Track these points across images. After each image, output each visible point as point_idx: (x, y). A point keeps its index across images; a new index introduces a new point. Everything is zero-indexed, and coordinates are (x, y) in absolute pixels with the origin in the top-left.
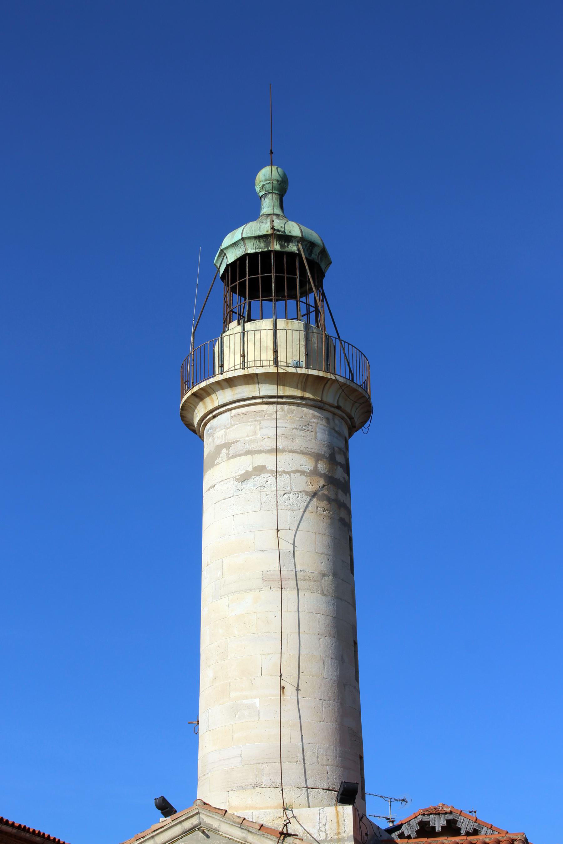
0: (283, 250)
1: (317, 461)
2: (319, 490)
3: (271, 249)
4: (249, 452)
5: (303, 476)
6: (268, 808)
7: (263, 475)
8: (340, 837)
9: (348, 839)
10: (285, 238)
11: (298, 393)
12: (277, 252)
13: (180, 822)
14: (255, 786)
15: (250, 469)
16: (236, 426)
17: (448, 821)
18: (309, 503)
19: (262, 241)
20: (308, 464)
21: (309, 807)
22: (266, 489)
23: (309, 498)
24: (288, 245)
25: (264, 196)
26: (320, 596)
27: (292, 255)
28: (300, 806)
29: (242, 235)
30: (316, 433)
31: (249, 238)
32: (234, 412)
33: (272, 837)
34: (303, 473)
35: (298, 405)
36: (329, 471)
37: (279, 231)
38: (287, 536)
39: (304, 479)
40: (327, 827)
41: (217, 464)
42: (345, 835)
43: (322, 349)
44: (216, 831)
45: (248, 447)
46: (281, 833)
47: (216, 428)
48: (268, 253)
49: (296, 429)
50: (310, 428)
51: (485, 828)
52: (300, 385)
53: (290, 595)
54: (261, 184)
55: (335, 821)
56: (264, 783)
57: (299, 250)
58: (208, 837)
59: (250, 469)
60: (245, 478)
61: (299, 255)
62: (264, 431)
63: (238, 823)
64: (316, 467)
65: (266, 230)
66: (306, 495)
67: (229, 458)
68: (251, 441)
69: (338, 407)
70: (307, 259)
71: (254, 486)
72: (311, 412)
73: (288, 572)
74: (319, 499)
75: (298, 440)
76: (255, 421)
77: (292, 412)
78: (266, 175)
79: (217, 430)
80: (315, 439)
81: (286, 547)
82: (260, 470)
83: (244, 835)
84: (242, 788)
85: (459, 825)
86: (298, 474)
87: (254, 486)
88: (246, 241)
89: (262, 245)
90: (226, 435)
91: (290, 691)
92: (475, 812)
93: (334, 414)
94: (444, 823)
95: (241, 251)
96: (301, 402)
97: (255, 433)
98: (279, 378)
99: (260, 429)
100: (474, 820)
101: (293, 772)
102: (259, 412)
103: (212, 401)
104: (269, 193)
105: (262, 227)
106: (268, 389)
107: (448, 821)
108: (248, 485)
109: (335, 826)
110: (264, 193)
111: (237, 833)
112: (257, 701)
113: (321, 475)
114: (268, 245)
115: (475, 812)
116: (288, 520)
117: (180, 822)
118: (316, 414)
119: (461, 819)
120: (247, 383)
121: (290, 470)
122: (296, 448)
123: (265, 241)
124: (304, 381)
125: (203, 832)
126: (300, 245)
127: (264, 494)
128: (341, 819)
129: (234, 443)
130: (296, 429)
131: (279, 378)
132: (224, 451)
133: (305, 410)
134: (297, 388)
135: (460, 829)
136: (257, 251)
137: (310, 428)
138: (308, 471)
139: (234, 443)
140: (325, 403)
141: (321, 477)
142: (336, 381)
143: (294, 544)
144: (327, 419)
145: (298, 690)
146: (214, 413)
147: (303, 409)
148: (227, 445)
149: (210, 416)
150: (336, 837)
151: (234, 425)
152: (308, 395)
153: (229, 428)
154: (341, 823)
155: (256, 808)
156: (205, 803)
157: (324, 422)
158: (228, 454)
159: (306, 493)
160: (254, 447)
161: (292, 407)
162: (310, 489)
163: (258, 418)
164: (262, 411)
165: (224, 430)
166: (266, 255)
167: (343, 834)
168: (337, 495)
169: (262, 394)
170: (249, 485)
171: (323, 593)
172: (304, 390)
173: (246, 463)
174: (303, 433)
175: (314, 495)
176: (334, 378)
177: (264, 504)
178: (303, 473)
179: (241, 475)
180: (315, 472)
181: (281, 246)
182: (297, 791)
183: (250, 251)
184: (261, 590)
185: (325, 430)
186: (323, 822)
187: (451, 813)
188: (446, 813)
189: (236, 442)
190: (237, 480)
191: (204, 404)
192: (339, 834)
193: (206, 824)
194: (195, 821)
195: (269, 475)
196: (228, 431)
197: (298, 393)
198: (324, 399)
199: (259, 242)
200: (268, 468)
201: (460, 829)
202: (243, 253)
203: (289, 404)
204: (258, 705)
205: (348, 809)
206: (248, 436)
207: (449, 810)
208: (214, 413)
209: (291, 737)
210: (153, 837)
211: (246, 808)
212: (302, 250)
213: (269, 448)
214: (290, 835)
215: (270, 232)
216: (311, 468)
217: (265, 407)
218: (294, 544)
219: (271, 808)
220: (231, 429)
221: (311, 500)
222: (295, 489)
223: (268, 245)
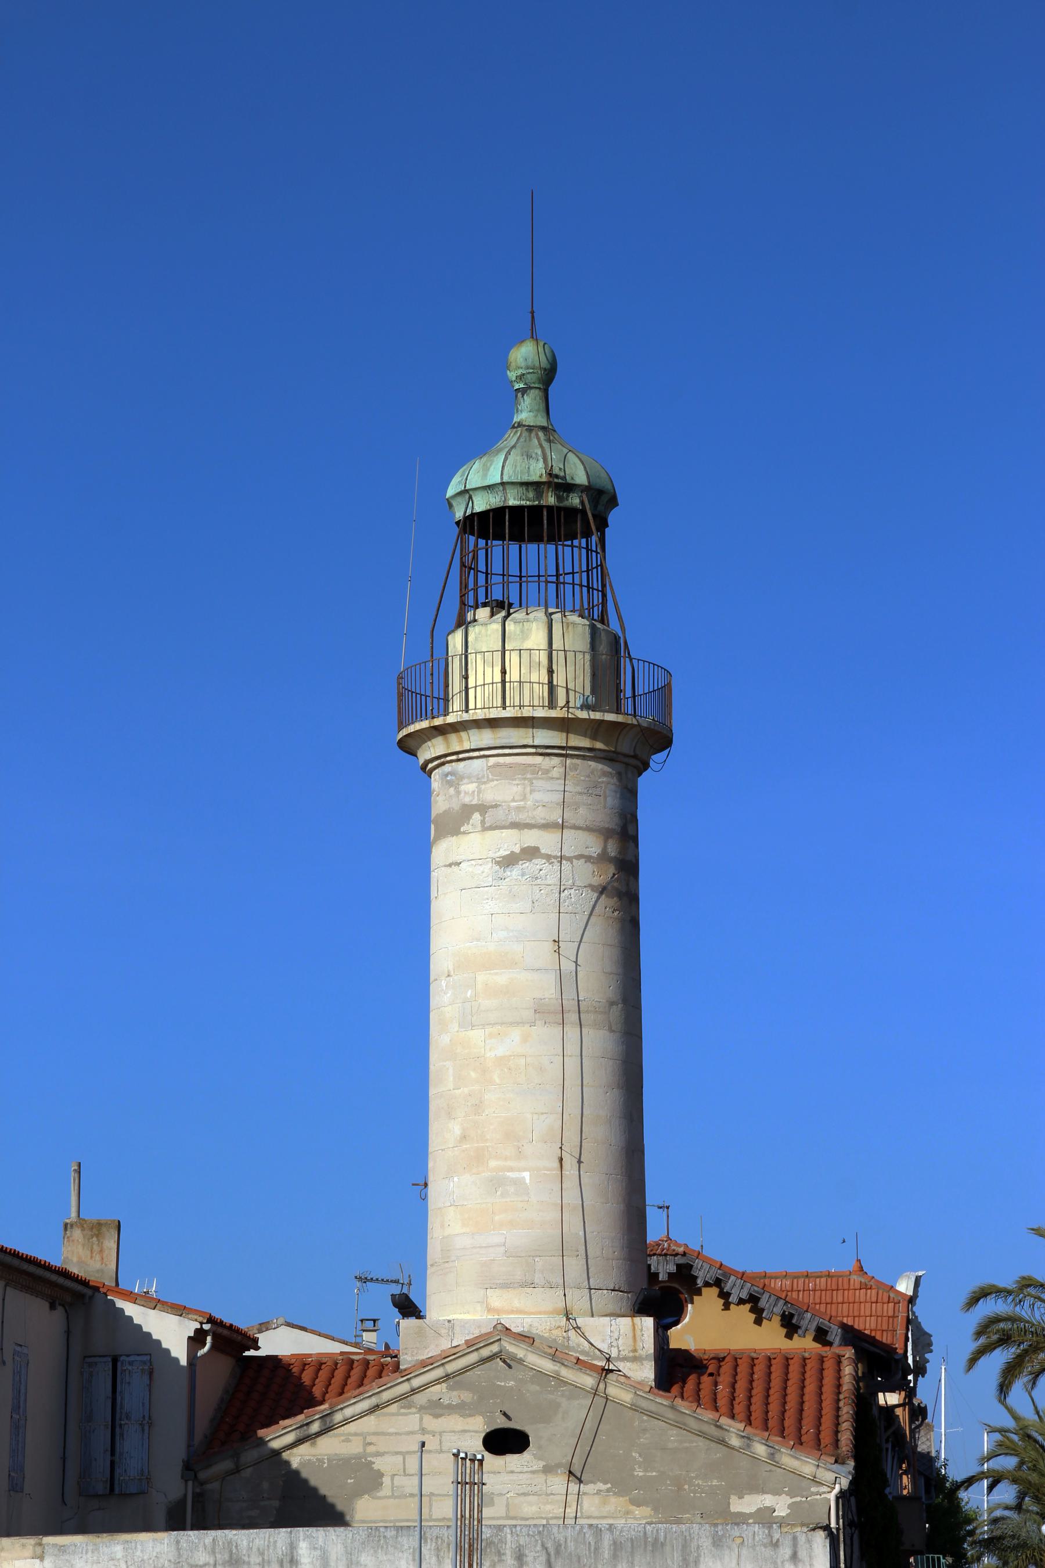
0: (561, 505)
1: (606, 842)
2: (608, 883)
3: (543, 503)
4: (515, 825)
5: (588, 864)
6: (540, 1313)
7: (535, 861)
8: (637, 1354)
9: (647, 1358)
10: (565, 487)
11: (585, 743)
12: (550, 508)
13: (477, 1349)
14: (524, 1285)
15: (517, 850)
16: (495, 782)
17: (678, 1266)
18: (596, 902)
19: (530, 488)
20: (593, 845)
21: (593, 1316)
22: (539, 881)
23: (596, 895)
24: (568, 496)
25: (523, 391)
26: (607, 1033)
27: (571, 512)
28: (584, 1315)
29: (502, 478)
30: (605, 797)
31: (513, 483)
32: (492, 760)
33: (591, 1373)
34: (588, 859)
35: (584, 757)
36: (620, 853)
37: (557, 476)
38: (568, 949)
39: (590, 867)
40: (620, 1342)
41: (464, 833)
42: (643, 1353)
43: (608, 658)
44: (520, 1361)
45: (514, 817)
46: (603, 1369)
47: (462, 778)
48: (539, 508)
49: (580, 793)
50: (598, 791)
51: (733, 1278)
52: (589, 732)
53: (572, 1033)
54: (519, 372)
55: (631, 1335)
56: (536, 1281)
57: (582, 503)
58: (510, 1367)
59: (517, 850)
60: (509, 861)
61: (583, 512)
62: (538, 796)
63: (550, 1354)
64: (605, 849)
65: (538, 474)
66: (593, 890)
67: (485, 829)
68: (518, 809)
69: (635, 757)
70: (594, 516)
71: (523, 875)
72: (600, 766)
73: (570, 1004)
74: (607, 896)
75: (582, 811)
76: (525, 779)
77: (575, 768)
78: (524, 355)
79: (465, 781)
80: (605, 807)
81: (568, 966)
82: (531, 853)
83: (556, 1368)
84: (506, 1286)
85: (694, 1273)
86: (583, 861)
87: (523, 875)
88: (507, 487)
89: (531, 495)
90: (479, 792)
91: (570, 1163)
92: (668, 1208)
93: (627, 764)
94: (672, 1268)
95: (498, 499)
96: (589, 755)
97: (524, 798)
98: (564, 725)
99: (532, 791)
100: (718, 1266)
101: (575, 1267)
102: (530, 765)
103: (461, 741)
104: (531, 388)
105: (532, 468)
106: (544, 737)
107: (678, 1266)
108: (514, 873)
109: (630, 1341)
110: (522, 386)
111: (547, 1366)
112: (526, 1175)
113: (611, 860)
114: (539, 495)
115: (668, 1208)
116: (570, 929)
117: (477, 1349)
118: (607, 769)
119: (697, 1263)
120: (518, 727)
121: (572, 855)
122: (580, 822)
123: (535, 490)
124: (594, 729)
125: (504, 1362)
126: (584, 496)
127: (536, 888)
128: (638, 1333)
129: (492, 807)
130: (580, 793)
131: (564, 725)
132: (476, 817)
133: (592, 763)
134: (585, 735)
135: (696, 1277)
136: (523, 503)
137: (598, 791)
138: (595, 855)
139: (492, 807)
140: (618, 753)
141: (610, 862)
142: (639, 725)
143: (576, 962)
144: (619, 774)
145: (580, 1162)
146: (461, 756)
147: (590, 763)
148: (483, 809)
149: (454, 757)
150: (631, 1354)
151: (493, 780)
152: (599, 745)
153: (485, 783)
154: (638, 1338)
155: (525, 1313)
156: (507, 1329)
157: (615, 780)
158: (483, 822)
159: (591, 887)
160: (522, 817)
161: (578, 761)
162: (597, 881)
163: (529, 776)
164: (534, 765)
165: (475, 785)
166: (535, 511)
167: (640, 1352)
168: (628, 885)
169: (536, 744)
170: (514, 872)
171: (611, 1030)
172: (594, 738)
173: (509, 841)
174: (589, 800)
175: (603, 890)
176: (635, 722)
177: (536, 904)
178: (588, 859)
179: (504, 857)
180: (603, 857)
181: (559, 498)
182: (577, 1292)
183: (512, 502)
184: (532, 1024)
185: (616, 792)
186: (616, 1335)
187: (684, 1254)
188: (677, 1255)
189: (496, 806)
190: (498, 863)
191: (447, 741)
192: (635, 1351)
193: (508, 1353)
194: (495, 1348)
195: (544, 861)
196: (483, 787)
197: (585, 743)
198: (619, 750)
199: (527, 490)
200: (543, 851)
201: (696, 1277)
202: (502, 504)
203: (572, 756)
204: (528, 1181)
205: (649, 1322)
206: (513, 800)
207: (681, 1250)
208: (461, 756)
209: (574, 1225)
210: (443, 1364)
211: (512, 1312)
212: (588, 507)
213: (543, 822)
214: (612, 1371)
215: (544, 479)
216: (599, 851)
217: (539, 759)
218: (576, 962)
219: (545, 1313)
220: (488, 786)
221: (598, 898)
222: (578, 883)
223: (539, 495)
